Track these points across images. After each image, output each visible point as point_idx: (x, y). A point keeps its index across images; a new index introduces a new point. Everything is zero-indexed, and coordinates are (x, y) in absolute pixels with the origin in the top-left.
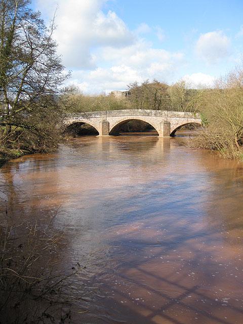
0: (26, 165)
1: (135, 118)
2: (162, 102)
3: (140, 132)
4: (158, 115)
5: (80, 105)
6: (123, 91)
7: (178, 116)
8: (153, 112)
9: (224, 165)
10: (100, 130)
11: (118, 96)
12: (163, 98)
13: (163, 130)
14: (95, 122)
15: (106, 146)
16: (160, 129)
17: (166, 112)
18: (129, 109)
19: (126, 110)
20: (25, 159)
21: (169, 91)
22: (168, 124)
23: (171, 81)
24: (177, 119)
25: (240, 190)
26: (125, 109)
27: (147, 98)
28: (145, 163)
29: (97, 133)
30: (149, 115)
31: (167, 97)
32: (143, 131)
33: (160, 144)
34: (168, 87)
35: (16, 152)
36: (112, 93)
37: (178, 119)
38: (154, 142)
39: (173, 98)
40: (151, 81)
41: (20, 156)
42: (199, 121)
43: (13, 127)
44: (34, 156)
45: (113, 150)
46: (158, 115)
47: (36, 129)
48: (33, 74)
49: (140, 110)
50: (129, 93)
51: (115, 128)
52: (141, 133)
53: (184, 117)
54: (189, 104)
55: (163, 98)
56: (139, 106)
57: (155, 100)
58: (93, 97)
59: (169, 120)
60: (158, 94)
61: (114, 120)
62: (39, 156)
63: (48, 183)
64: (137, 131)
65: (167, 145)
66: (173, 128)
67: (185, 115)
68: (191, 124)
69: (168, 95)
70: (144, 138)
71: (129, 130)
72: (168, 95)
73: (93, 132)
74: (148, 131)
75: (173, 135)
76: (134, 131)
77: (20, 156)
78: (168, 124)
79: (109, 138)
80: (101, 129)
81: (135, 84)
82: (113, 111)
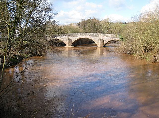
0: (30, 62)
1: (85, 37)
2: (98, 29)
3: (86, 44)
4: (97, 36)
5: (61, 31)
6: (76, 23)
7: (108, 36)
8: (95, 34)
9: (136, 63)
10: (66, 44)
11: (74, 26)
12: (98, 27)
13: (100, 44)
14: (64, 39)
15: (69, 52)
16: (98, 43)
17: (101, 34)
18: (82, 32)
19: (80, 33)
20: (30, 59)
21: (101, 23)
22: (102, 40)
23: (102, 18)
24: (107, 38)
25: (155, 76)
26: (79, 32)
27: (90, 27)
28: (95, 62)
29: (65, 45)
30: (92, 36)
31: (100, 26)
32: (88, 44)
33: (98, 51)
34: (100, 22)
35: (26, 55)
36: (71, 24)
37: (108, 38)
38: (93, 51)
39: (103, 27)
40: (92, 18)
41: (27, 58)
42: (118, 39)
43: (24, 42)
44: (34, 58)
45: (74, 55)
46: (97, 36)
47: (38, 43)
48: (35, 14)
49: (88, 33)
50: (80, 24)
51: (74, 43)
52: (87, 45)
53: (111, 37)
54: (111, 30)
55: (98, 27)
56: (86, 31)
57: (94, 28)
58: (131, 22)
59: (103, 38)
60: (96, 25)
61: (74, 38)
62: (37, 57)
63: (44, 72)
64: (85, 44)
65: (102, 53)
66: (105, 42)
67: (111, 36)
68: (113, 41)
69: (101, 25)
70: (88, 48)
71: (81, 43)
72: (101, 25)
73: (63, 45)
74: (90, 44)
75: (105, 46)
76: (83, 44)
77: (27, 58)
78: (102, 40)
79: (71, 47)
80: (67, 43)
81: (84, 20)
82: (73, 34)
